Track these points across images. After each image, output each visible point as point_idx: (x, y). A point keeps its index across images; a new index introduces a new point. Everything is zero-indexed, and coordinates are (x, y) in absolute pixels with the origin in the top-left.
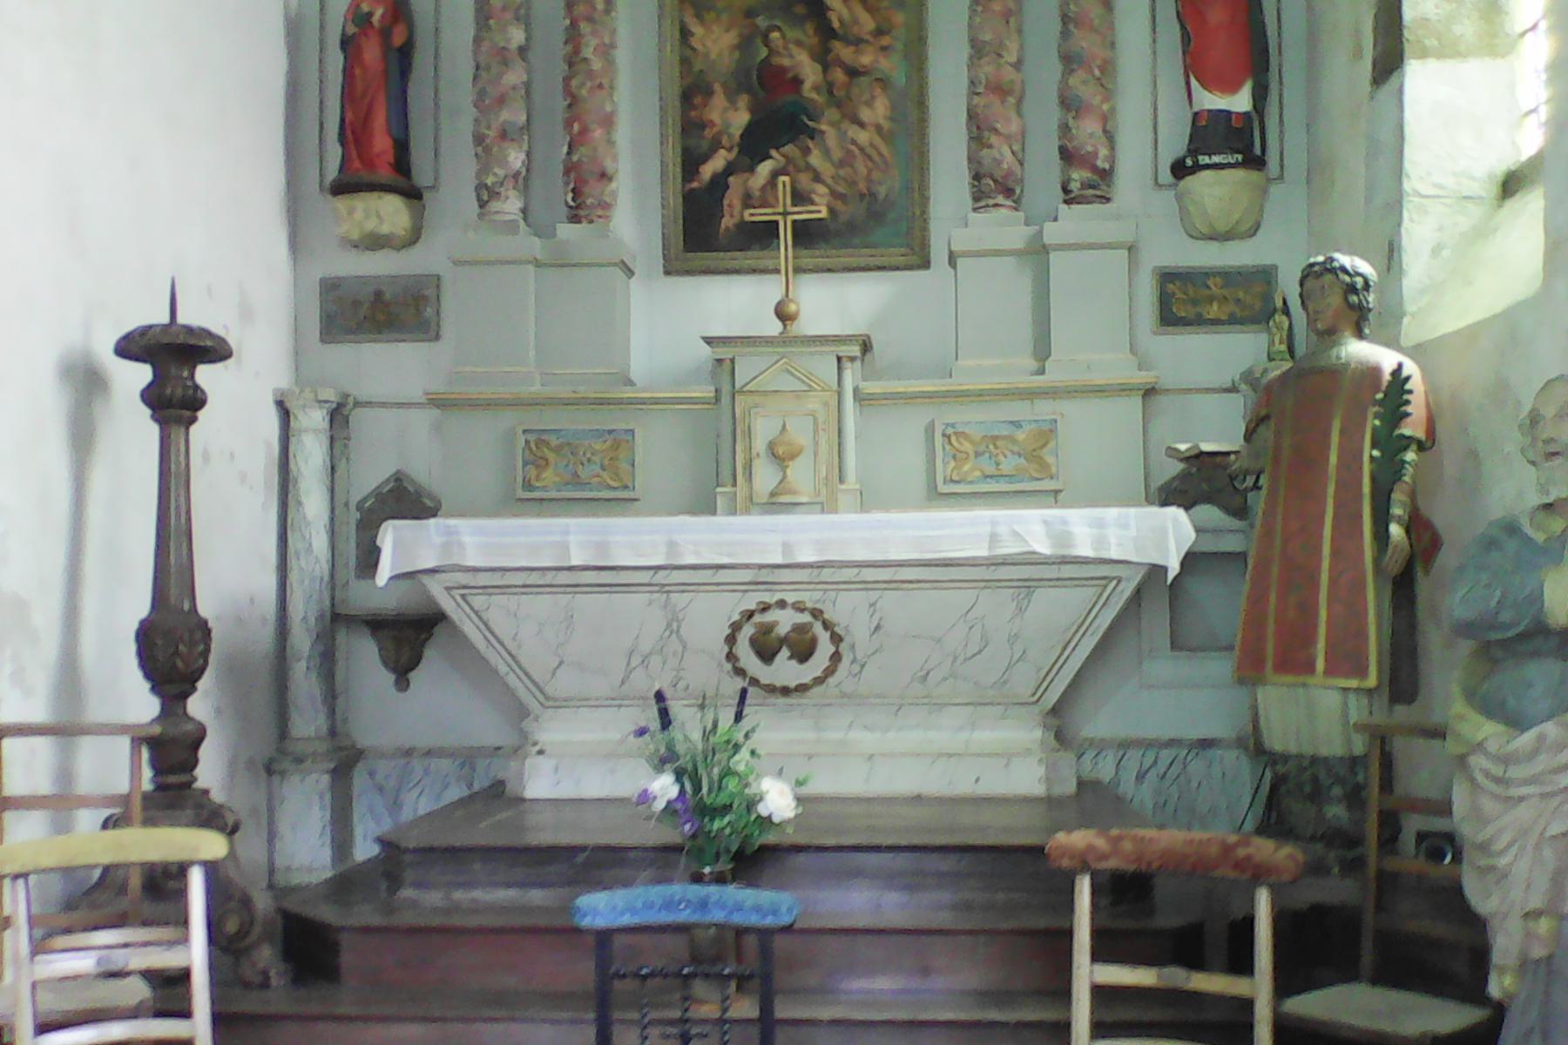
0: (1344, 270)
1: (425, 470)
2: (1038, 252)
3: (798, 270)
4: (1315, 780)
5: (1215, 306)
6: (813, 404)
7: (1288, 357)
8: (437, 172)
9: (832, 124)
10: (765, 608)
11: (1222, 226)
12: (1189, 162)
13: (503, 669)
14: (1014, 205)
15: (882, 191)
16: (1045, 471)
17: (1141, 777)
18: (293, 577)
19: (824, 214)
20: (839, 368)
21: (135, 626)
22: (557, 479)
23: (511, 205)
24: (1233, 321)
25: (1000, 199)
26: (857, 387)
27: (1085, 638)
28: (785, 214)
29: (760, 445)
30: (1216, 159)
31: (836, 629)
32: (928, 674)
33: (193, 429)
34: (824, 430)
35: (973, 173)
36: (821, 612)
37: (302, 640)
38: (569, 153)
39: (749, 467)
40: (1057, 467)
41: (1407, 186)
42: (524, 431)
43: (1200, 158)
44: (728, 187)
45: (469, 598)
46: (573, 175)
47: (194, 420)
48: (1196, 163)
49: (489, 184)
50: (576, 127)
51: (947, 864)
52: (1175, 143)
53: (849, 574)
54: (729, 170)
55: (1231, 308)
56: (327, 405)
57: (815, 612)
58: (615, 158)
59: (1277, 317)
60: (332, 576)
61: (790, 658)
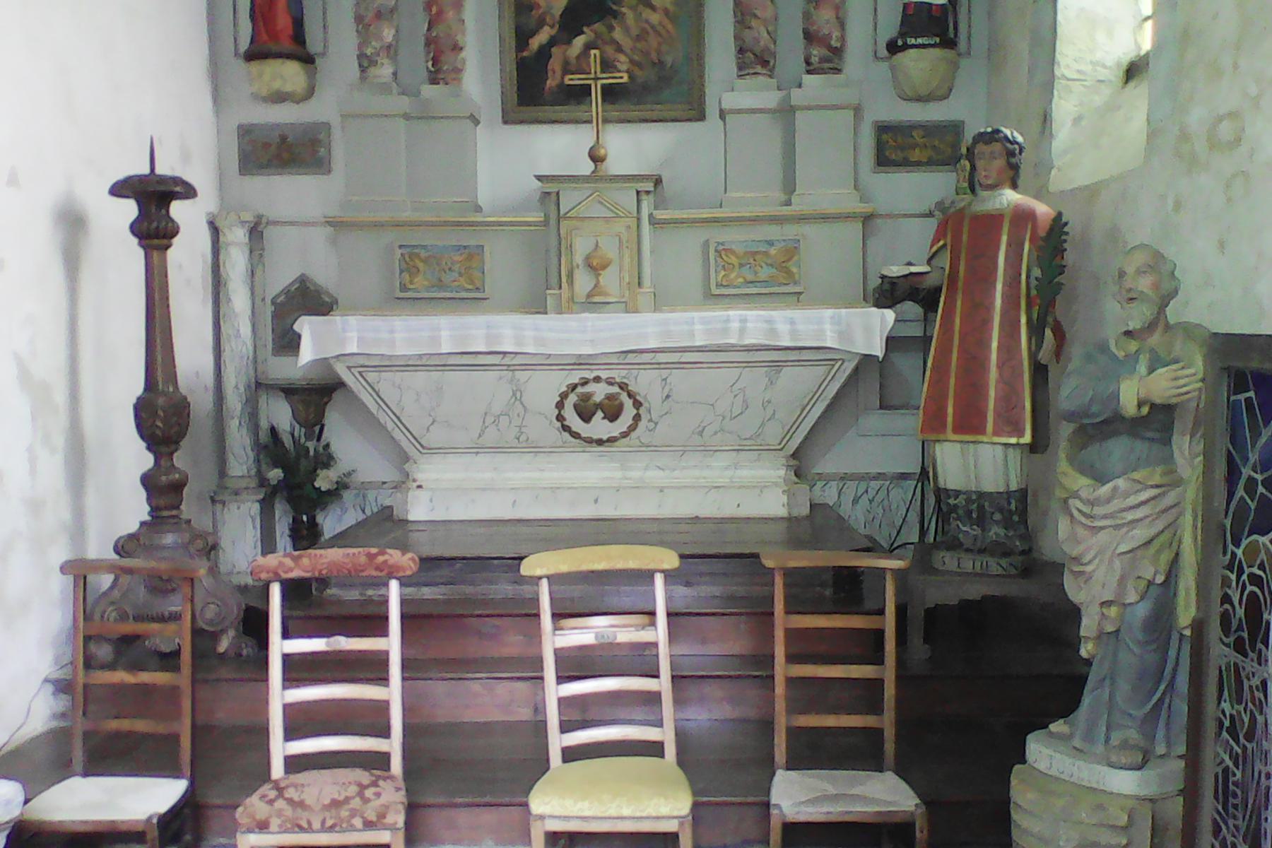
0: (1006, 138)
1: (325, 275)
2: (786, 112)
3: (606, 121)
4: (981, 508)
5: (917, 150)
6: (619, 227)
7: (969, 191)
8: (325, 40)
9: (631, 8)
10: (585, 382)
11: (924, 91)
12: (900, 43)
13: (390, 426)
14: (769, 73)
15: (669, 60)
16: (790, 277)
17: (856, 501)
18: (226, 356)
19: (625, 79)
20: (639, 201)
21: (134, 401)
22: (426, 283)
23: (384, 71)
24: (931, 163)
25: (759, 69)
26: (652, 214)
27: (818, 402)
28: (596, 79)
29: (579, 259)
30: (920, 41)
31: (638, 398)
32: (704, 429)
33: (170, 252)
34: (627, 247)
35: (738, 48)
36: (627, 385)
37: (234, 402)
38: (429, 29)
39: (570, 275)
40: (800, 274)
41: (1057, 72)
42: (401, 247)
43: (908, 40)
44: (551, 57)
45: (364, 374)
46: (432, 46)
47: (168, 246)
48: (905, 44)
49: (369, 54)
50: (434, 10)
51: (718, 566)
52: (890, 26)
53: (646, 358)
54: (552, 42)
55: (929, 153)
56: (247, 224)
57: (623, 385)
58: (463, 33)
59: (962, 161)
60: (255, 357)
61: (604, 418)
